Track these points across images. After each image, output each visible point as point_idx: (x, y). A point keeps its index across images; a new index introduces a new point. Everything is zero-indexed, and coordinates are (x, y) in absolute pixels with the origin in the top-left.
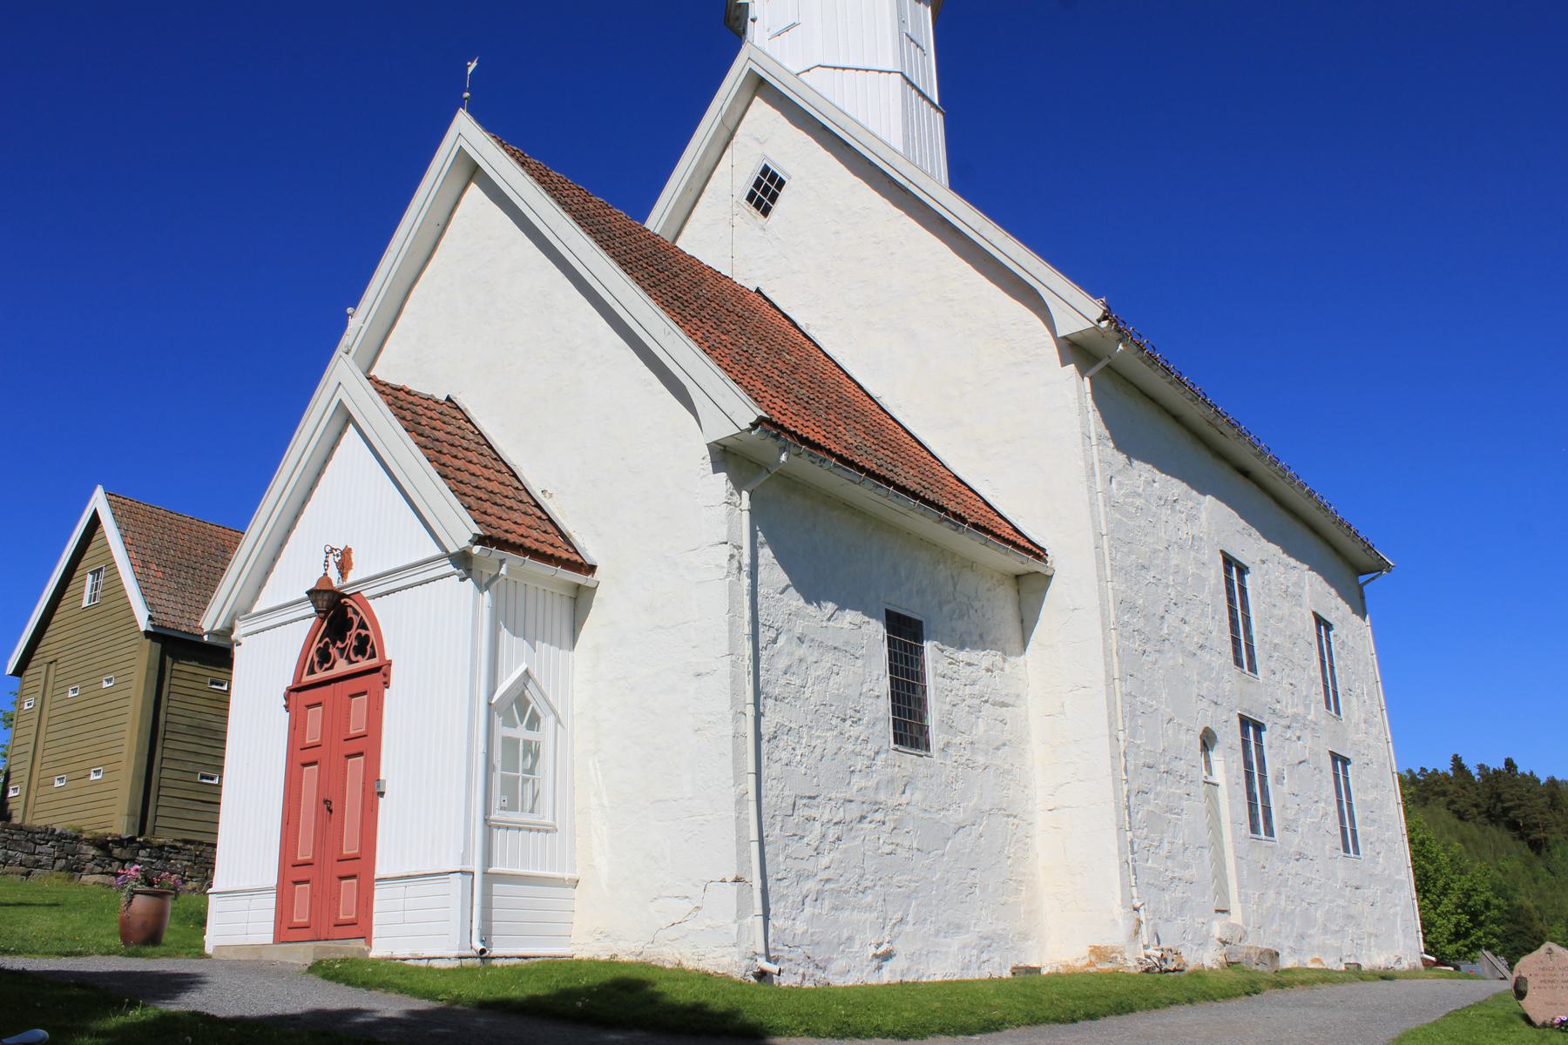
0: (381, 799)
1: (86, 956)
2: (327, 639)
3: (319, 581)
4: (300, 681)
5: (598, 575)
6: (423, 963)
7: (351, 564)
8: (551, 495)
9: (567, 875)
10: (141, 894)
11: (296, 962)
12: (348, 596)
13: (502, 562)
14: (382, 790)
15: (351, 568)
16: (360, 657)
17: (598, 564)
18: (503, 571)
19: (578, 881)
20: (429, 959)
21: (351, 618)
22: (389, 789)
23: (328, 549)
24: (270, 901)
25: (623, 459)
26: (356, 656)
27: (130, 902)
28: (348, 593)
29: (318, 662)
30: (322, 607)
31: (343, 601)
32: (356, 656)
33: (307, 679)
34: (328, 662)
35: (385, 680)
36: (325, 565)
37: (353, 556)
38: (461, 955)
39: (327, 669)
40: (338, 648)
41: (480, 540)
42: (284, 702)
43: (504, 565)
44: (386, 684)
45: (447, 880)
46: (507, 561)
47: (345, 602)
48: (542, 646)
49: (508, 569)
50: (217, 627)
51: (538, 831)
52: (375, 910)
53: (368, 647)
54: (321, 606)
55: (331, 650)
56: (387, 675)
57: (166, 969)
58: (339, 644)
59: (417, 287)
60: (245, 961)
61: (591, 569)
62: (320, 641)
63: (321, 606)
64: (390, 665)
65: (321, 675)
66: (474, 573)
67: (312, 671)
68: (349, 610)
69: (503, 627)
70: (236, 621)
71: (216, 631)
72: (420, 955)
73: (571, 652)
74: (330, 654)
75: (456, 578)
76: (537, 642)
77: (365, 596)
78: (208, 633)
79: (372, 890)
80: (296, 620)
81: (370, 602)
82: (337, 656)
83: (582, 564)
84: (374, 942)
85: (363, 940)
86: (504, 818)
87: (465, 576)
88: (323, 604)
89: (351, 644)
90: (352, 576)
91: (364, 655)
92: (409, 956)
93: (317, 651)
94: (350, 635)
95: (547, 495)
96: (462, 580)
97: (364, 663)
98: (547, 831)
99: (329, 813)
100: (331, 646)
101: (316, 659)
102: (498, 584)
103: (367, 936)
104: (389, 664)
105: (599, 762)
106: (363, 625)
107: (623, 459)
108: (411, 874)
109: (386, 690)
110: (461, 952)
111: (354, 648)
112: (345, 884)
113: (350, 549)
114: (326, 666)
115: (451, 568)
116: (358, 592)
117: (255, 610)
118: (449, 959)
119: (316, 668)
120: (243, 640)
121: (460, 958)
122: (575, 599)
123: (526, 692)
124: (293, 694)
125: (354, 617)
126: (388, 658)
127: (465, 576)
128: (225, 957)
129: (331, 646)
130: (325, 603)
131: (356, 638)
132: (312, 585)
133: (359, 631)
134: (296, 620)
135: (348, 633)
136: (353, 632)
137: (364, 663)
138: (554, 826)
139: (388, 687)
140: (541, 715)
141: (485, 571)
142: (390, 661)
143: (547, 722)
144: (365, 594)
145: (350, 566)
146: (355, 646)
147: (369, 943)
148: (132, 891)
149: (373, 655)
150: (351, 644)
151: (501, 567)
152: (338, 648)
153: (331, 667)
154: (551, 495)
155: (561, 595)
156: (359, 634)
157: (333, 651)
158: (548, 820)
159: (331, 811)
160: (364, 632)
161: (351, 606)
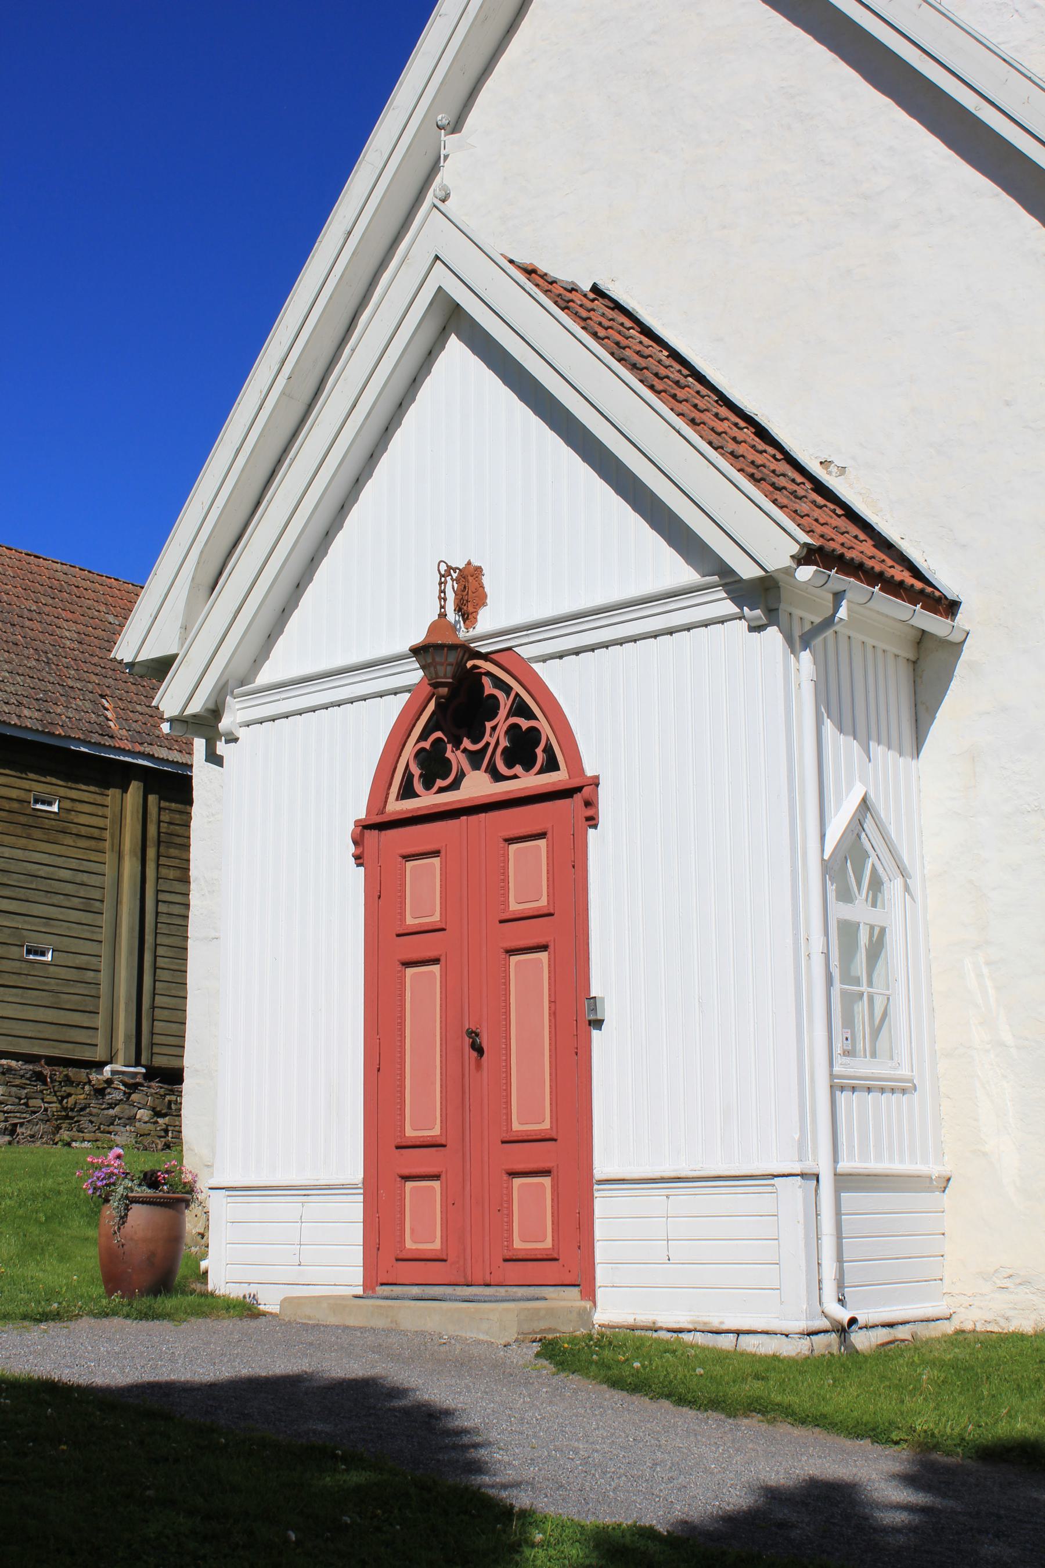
0: (595, 1033)
1: (70, 1319)
2: (439, 734)
3: (433, 628)
4: (382, 811)
5: (962, 618)
6: (726, 1342)
7: (485, 596)
8: (842, 470)
9: (934, 1169)
10: (143, 1203)
11: (482, 1337)
12: (485, 657)
13: (838, 597)
14: (599, 1017)
15: (484, 604)
16: (518, 769)
17: (962, 599)
18: (842, 613)
19: (949, 1180)
20: (738, 1333)
21: (493, 697)
22: (609, 1013)
23: (443, 568)
24: (354, 1208)
25: (1008, 404)
26: (510, 765)
27: (123, 1218)
28: (483, 650)
29: (421, 776)
30: (445, 677)
31: (469, 664)
32: (510, 765)
33: (396, 807)
34: (444, 777)
35: (589, 812)
36: (440, 598)
37: (486, 580)
38: (811, 1329)
39: (441, 790)
40: (465, 751)
41: (808, 556)
42: (352, 848)
43: (844, 603)
44: (592, 821)
45: (769, 1189)
46: (848, 595)
47: (475, 667)
48: (878, 750)
49: (849, 610)
50: (196, 707)
51: (869, 1090)
52: (598, 1235)
53: (539, 751)
54: (441, 674)
55: (449, 754)
56: (590, 803)
57: (326, 1366)
58: (467, 743)
59: (490, 83)
60: (362, 1329)
61: (950, 607)
62: (423, 737)
63: (441, 674)
64: (597, 785)
65: (427, 800)
66: (783, 617)
67: (407, 792)
68: (486, 681)
69: (825, 715)
70: (228, 698)
71: (194, 716)
72: (715, 1323)
73: (915, 761)
74: (449, 761)
75: (744, 624)
76: (871, 743)
77: (525, 656)
78: (172, 721)
79: (591, 1199)
80: (364, 698)
81: (537, 667)
82: (466, 765)
83: (940, 598)
84: (600, 1293)
85: (576, 1290)
86: (850, 1071)
87: (764, 621)
88: (446, 673)
89: (497, 743)
90: (487, 621)
91: (528, 765)
92: (691, 1327)
93: (417, 755)
94: (494, 728)
95: (835, 470)
96: (756, 628)
97: (529, 781)
98: (904, 1091)
99: (474, 1054)
100: (449, 746)
101: (416, 771)
102: (825, 638)
103: (586, 1285)
104: (595, 782)
105: (988, 964)
106: (521, 709)
107: (1008, 404)
108: (683, 1174)
109: (591, 832)
110: (810, 1323)
111: (503, 753)
112: (521, 1186)
113: (479, 570)
114: (440, 783)
115: (729, 607)
116: (509, 649)
117: (266, 676)
118: (787, 1336)
119: (418, 786)
120: (242, 733)
121: (810, 1334)
122: (914, 663)
123: (863, 836)
124: (371, 835)
125: (500, 695)
126: (589, 772)
127: (764, 621)
128: (310, 1318)
129: (449, 746)
130: (449, 668)
131: (506, 733)
132: (418, 637)
133: (514, 720)
134: (364, 698)
135: (489, 725)
136: (502, 721)
137: (529, 781)
138: (911, 1081)
139: (595, 826)
140: (885, 878)
141: (798, 612)
142: (597, 777)
143: (893, 888)
144: (525, 652)
145: (481, 600)
146: (505, 749)
147: (589, 1293)
148: (127, 1197)
149: (552, 765)
150: (497, 743)
151: (836, 608)
152: (465, 751)
153: (455, 785)
154: (842, 470)
155: (896, 656)
156: (515, 727)
157: (456, 757)
158: (904, 1072)
159: (479, 1050)
160: (525, 724)
161: (488, 674)
